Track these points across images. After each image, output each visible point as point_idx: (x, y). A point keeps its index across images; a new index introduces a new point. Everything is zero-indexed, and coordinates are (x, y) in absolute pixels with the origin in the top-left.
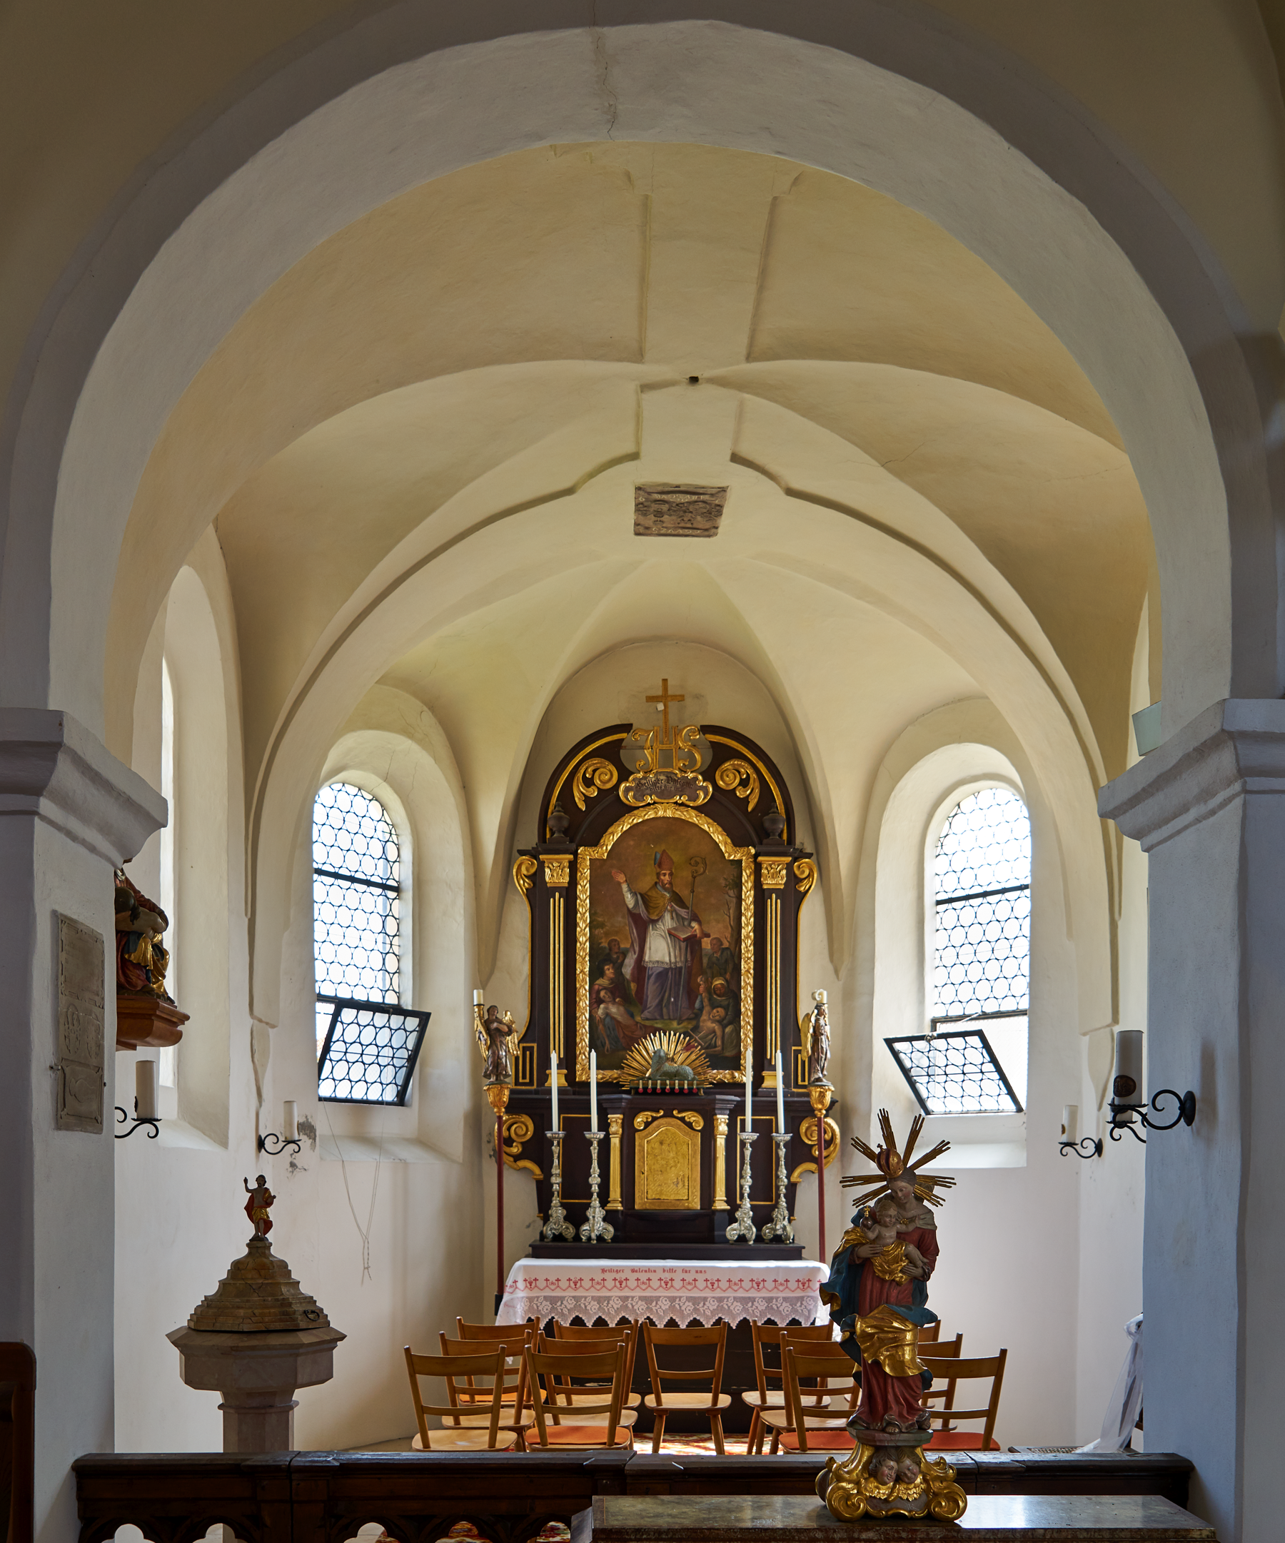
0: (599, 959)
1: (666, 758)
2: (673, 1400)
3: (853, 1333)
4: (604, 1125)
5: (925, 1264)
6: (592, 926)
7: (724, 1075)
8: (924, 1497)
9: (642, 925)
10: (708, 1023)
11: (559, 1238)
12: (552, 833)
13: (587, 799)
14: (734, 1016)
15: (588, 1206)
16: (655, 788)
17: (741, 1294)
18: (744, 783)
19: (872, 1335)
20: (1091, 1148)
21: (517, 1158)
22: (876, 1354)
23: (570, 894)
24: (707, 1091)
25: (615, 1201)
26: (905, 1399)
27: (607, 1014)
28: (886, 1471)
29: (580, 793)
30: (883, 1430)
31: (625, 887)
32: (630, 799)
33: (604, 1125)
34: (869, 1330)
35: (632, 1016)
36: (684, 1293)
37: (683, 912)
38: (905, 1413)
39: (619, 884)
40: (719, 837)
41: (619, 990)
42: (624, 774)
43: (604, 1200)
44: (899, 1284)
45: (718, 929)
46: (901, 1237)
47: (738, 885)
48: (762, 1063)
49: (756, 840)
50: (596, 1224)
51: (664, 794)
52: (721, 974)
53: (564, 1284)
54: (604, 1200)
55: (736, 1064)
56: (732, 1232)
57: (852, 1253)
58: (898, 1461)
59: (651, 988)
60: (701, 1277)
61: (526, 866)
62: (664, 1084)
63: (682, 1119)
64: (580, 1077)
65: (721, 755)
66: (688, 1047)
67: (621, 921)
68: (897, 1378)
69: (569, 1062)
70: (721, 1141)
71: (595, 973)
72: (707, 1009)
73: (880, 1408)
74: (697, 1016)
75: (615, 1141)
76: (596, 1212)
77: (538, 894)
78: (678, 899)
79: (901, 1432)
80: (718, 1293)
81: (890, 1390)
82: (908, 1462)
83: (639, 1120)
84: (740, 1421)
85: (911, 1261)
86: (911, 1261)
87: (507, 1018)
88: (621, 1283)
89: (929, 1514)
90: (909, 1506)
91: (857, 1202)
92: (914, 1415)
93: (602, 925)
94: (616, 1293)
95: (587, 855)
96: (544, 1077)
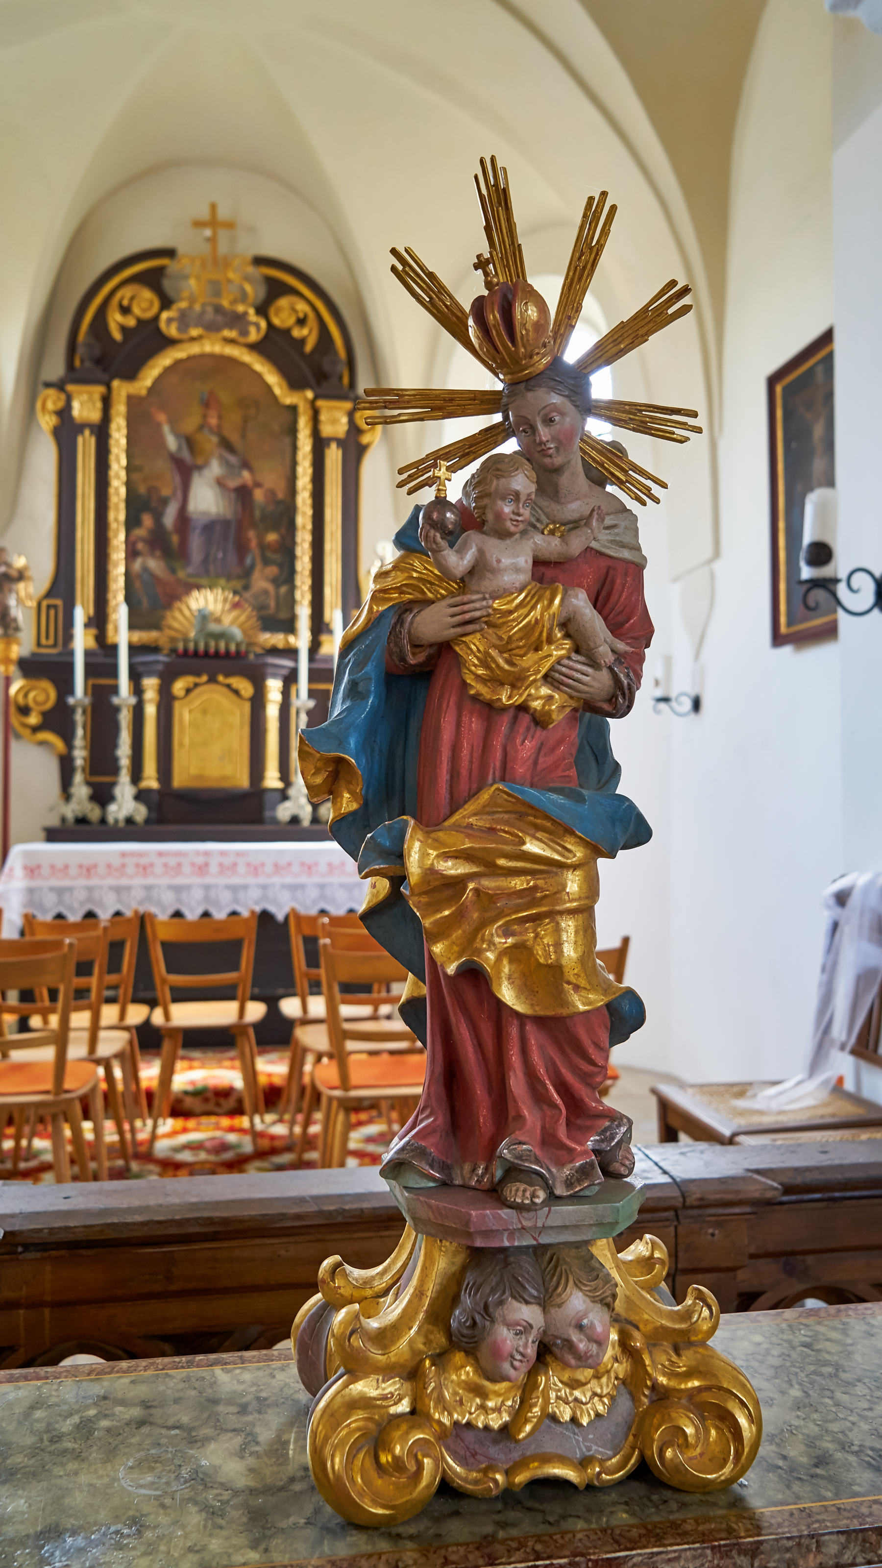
0: (137, 506)
1: (216, 289)
2: (189, 1015)
3: (398, 880)
4: (138, 690)
5: (620, 657)
6: (129, 469)
7: (277, 639)
8: (624, 1403)
9: (185, 471)
10: (261, 581)
11: (82, 820)
12: (82, 361)
13: (123, 329)
14: (287, 575)
15: (113, 784)
16: (200, 321)
17: (289, 880)
18: (301, 322)
19: (457, 884)
20: (688, 704)
21: (35, 729)
22: (469, 943)
23: (102, 432)
24: (257, 656)
25: (149, 778)
26: (564, 1089)
27: (145, 569)
28: (505, 1336)
29: (115, 320)
30: (494, 1193)
31: (166, 429)
32: (172, 331)
33: (138, 690)
34: (451, 868)
35: (173, 571)
36: (223, 881)
37: (232, 459)
38: (562, 1132)
39: (159, 426)
40: (272, 378)
41: (158, 542)
42: (166, 303)
43: (136, 776)
44: (540, 721)
45: (270, 478)
46: (546, 571)
47: (293, 431)
48: (319, 626)
49: (312, 380)
50: (125, 804)
51: (212, 328)
52: (275, 527)
53: (73, 871)
54: (136, 776)
55: (290, 626)
56: (284, 812)
57: (394, 633)
58: (546, 1302)
59: (196, 542)
60: (241, 861)
61: (52, 400)
62: (207, 645)
63: (229, 686)
64: (111, 637)
65: (276, 290)
66: (236, 606)
67: (162, 465)
68: (540, 1021)
69: (99, 620)
70: (272, 711)
71: (132, 522)
72: (259, 567)
73: (483, 1115)
74: (247, 574)
75: (151, 710)
76: (124, 790)
77: (66, 431)
78: (226, 445)
79: (553, 1198)
80: (262, 880)
81: (514, 1057)
82: (576, 1302)
83: (179, 686)
84: (276, 1033)
85: (581, 647)
86: (581, 647)
87: (20, 562)
88: (145, 869)
89: (644, 1473)
90: (579, 1446)
91: (416, 474)
92: (587, 1130)
93: (139, 469)
94: (139, 881)
95: (121, 389)
96: (69, 637)
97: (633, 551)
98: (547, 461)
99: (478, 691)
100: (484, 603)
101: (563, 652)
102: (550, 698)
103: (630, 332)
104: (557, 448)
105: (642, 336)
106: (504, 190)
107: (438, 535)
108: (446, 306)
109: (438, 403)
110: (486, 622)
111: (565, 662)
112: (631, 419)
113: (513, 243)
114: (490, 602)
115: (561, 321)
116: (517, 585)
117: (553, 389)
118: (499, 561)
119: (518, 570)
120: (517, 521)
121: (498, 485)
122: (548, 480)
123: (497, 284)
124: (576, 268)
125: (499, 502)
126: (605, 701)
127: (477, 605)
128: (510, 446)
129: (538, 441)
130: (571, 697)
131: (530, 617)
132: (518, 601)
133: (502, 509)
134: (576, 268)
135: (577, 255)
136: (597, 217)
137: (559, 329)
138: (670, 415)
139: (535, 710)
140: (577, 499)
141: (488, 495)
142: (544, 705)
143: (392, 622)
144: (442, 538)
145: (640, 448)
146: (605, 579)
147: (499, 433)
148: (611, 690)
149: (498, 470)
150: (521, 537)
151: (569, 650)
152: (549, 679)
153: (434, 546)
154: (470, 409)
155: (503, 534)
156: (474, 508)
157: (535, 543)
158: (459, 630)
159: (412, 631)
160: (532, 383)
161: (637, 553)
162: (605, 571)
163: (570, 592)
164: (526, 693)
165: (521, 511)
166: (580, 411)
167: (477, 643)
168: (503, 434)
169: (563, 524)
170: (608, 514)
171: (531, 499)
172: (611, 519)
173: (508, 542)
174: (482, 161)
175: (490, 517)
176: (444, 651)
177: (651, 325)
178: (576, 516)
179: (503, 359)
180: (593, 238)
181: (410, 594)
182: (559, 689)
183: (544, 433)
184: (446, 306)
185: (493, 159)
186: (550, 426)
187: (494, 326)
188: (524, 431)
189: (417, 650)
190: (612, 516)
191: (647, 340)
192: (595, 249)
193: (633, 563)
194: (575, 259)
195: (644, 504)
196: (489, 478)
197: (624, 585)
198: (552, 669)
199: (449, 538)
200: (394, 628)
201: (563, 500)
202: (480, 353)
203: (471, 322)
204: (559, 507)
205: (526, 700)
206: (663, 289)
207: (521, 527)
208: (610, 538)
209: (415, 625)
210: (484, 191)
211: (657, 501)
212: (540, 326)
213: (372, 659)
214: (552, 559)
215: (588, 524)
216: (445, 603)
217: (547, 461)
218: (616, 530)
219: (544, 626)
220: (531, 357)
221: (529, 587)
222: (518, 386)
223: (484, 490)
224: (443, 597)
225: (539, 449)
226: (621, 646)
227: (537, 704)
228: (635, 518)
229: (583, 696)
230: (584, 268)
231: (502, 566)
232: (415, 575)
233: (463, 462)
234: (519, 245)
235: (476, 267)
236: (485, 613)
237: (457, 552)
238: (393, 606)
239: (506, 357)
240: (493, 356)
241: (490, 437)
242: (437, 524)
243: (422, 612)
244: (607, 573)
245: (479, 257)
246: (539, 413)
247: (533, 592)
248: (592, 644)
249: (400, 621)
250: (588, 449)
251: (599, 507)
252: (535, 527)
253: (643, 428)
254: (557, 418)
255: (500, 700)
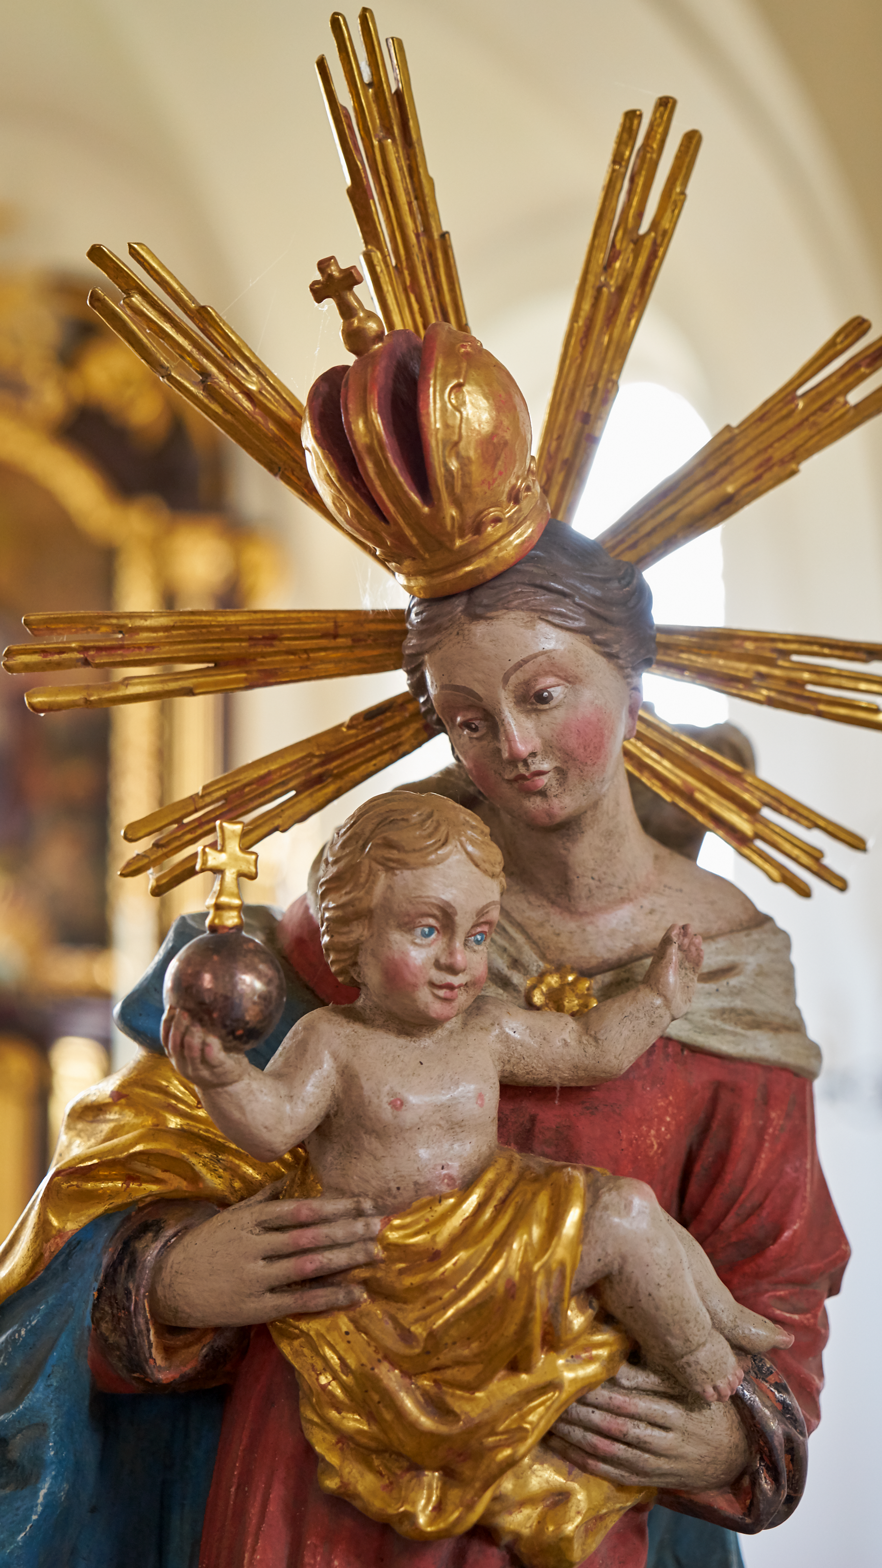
46: (538, 1116)
86: (645, 1345)
97: (783, 1036)
98: (535, 804)
99: (344, 1485)
100: (359, 1227)
101: (591, 1369)
102: (559, 1498)
103: (750, 452)
104: (561, 773)
105: (782, 462)
106: (399, 95)
107: (215, 1042)
108: (248, 394)
109: (233, 648)
110: (365, 1283)
111: (602, 1395)
112: (761, 676)
113: (427, 230)
114: (376, 1224)
115: (563, 426)
116: (455, 1169)
117: (543, 614)
118: (398, 1104)
119: (454, 1126)
120: (450, 987)
121: (390, 887)
122: (540, 860)
123: (379, 337)
124: (599, 290)
125: (397, 937)
126: (719, 1486)
127: (338, 1231)
128: (434, 757)
129: (506, 755)
130: (620, 1486)
131: (490, 1277)
132: (455, 1222)
133: (405, 954)
134: (599, 290)
135: (601, 258)
136: (648, 161)
137: (558, 448)
138: (865, 661)
139: (517, 1537)
140: (623, 900)
141: (366, 915)
142: (542, 1521)
143: (105, 1261)
144: (227, 1049)
145: (791, 751)
146: (710, 1117)
147: (405, 723)
148: (739, 1459)
149: (389, 845)
150: (465, 1024)
151: (611, 1363)
152: (555, 1443)
153: (205, 1073)
154: (322, 661)
155: (412, 1024)
156: (330, 947)
157: (506, 1039)
158: (287, 1301)
159: (160, 1292)
160: (484, 597)
161: (793, 1038)
162: (708, 1094)
163: (606, 1198)
164: (488, 1495)
165: (460, 958)
166: (621, 668)
167: (341, 1347)
168: (415, 726)
169: (585, 973)
170: (709, 937)
171: (489, 923)
172: (718, 952)
173: (427, 1042)
174: (336, 23)
175: (372, 975)
176: (242, 1361)
177: (805, 433)
178: (620, 947)
179: (400, 538)
180: (640, 215)
181: (157, 1181)
182: (584, 1468)
183: (522, 732)
184: (248, 394)
185: (365, 17)
186: (538, 711)
187: (370, 449)
188: (466, 725)
189: (179, 1340)
190: (721, 943)
191: (794, 473)
192: (648, 243)
193: (784, 1069)
194: (596, 267)
195: (804, 892)
196: (365, 869)
197: (761, 1133)
198: (565, 1418)
199: (248, 1047)
200: (110, 1278)
201: (583, 905)
202: (340, 518)
203: (308, 439)
204: (572, 925)
205: (489, 1513)
206: (832, 343)
207: (463, 999)
208: (719, 1003)
209: (166, 1276)
210: (345, 99)
211: (840, 884)
212: (499, 447)
213: (48, 1369)
214: (557, 1081)
215: (652, 980)
216: (246, 1215)
217: (535, 804)
218: (734, 981)
219: (530, 1305)
220: (478, 529)
221: (490, 1176)
222: (446, 607)
223: (350, 903)
224: (251, 1188)
225: (509, 775)
226: (760, 1331)
227: (520, 1521)
228: (784, 940)
229: (657, 1482)
230: (621, 290)
231: (408, 1117)
232: (174, 1122)
233: (306, 804)
234: (444, 236)
235: (319, 293)
236: (361, 1258)
237: (278, 1076)
238: (106, 1216)
239: (408, 532)
240: (380, 527)
241: (379, 735)
242: (209, 1012)
243: (188, 1239)
244: (714, 1100)
245: (323, 265)
246: (506, 680)
247: (500, 1194)
248: (676, 1344)
249: (126, 1259)
250: (651, 757)
251: (684, 927)
252: (505, 983)
253: (794, 698)
254: (558, 692)
255: (411, 1517)
